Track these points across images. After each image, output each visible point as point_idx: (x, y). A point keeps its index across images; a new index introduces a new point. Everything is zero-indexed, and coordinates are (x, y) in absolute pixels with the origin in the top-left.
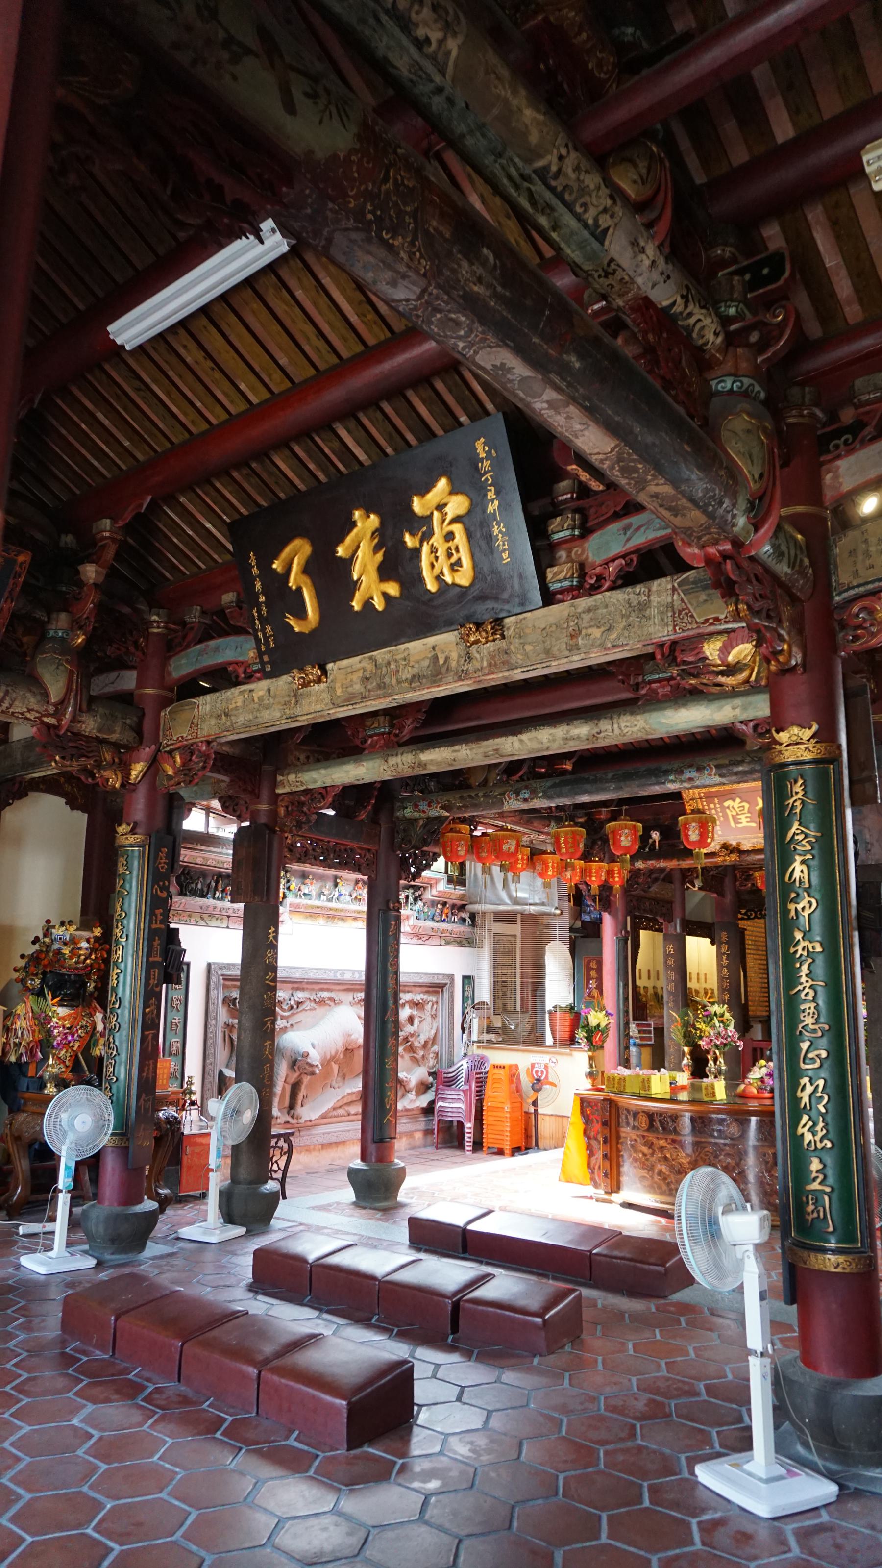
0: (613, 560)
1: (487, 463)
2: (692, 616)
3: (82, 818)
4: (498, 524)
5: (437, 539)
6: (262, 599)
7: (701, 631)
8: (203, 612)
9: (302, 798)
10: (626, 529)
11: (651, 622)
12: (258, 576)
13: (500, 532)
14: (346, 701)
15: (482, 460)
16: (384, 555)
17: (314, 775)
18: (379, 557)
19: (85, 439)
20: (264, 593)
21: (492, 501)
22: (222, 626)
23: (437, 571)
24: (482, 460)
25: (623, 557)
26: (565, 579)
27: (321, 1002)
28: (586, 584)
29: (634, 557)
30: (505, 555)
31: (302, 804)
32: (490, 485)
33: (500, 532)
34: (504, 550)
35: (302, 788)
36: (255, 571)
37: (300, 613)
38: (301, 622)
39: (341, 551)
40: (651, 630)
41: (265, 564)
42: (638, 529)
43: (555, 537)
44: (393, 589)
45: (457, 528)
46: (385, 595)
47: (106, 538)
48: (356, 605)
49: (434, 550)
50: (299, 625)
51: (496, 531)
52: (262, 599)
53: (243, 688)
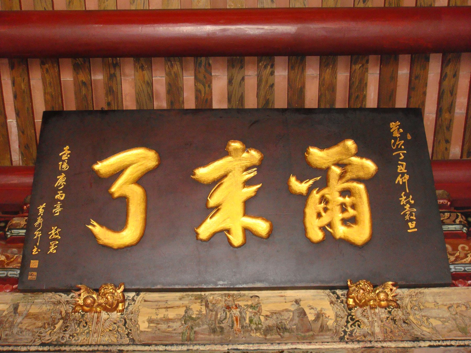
4: (407, 195)
5: (333, 192)
12: (65, 172)
14: (154, 338)
15: (395, 138)
18: (251, 190)
21: (403, 174)
23: (325, 219)
27: (298, 343)
30: (412, 225)
32: (402, 161)
33: (408, 202)
34: (411, 220)
44: (261, 226)
46: (247, 231)
48: (396, 182)
52: (60, 196)
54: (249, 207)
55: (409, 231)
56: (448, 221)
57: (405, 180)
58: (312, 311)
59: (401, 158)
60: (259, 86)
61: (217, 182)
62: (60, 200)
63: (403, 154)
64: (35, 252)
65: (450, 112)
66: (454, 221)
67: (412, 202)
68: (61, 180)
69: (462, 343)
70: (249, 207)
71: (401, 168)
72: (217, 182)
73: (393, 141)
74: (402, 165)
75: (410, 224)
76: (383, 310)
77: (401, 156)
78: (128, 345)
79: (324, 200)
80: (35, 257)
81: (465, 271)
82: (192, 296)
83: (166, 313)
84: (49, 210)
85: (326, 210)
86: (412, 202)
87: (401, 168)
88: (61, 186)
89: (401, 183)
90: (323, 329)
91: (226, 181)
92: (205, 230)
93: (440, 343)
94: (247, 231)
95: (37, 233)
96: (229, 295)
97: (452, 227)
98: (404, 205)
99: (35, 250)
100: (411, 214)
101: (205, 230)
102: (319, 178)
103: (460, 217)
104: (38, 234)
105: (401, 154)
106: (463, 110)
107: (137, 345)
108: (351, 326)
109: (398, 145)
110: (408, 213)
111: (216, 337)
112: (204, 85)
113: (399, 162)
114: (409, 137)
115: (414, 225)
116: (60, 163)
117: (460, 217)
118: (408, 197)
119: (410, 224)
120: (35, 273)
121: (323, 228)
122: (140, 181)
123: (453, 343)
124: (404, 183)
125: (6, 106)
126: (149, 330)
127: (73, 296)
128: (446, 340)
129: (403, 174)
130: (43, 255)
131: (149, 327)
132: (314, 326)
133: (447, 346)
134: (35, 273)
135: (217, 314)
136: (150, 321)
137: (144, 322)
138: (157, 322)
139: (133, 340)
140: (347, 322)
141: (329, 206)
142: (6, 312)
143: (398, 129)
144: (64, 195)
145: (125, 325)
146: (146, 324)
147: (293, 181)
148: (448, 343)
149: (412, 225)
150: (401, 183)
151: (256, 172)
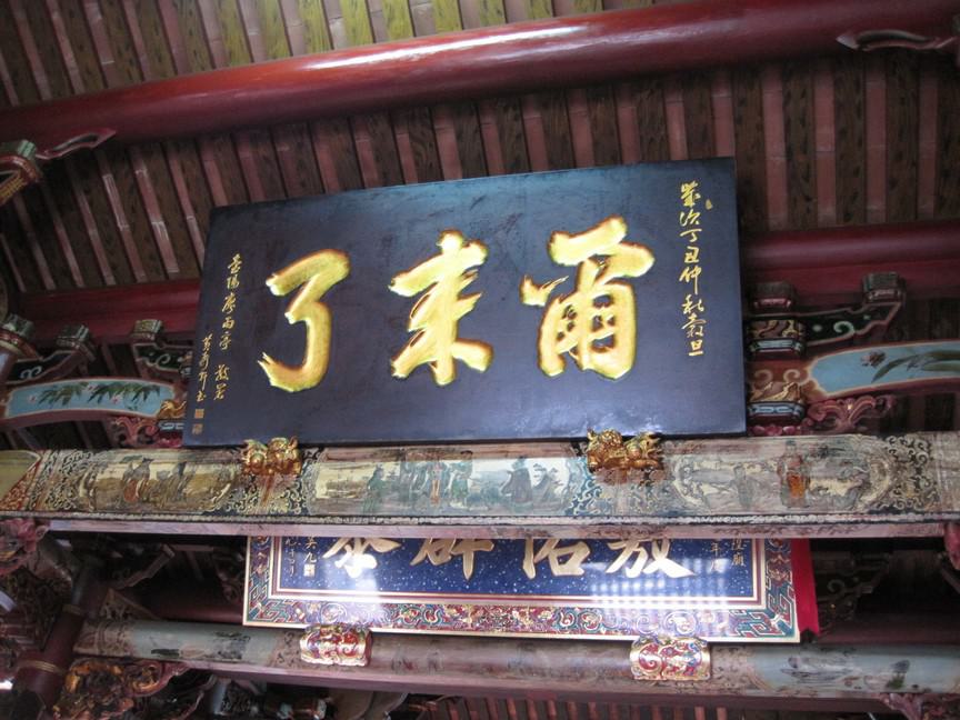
0: (856, 396)
1: (694, 216)
3: (585, 368)
5: (582, 301)
8: (89, 339)
9: (117, 670)
10: (876, 359)
13: (695, 310)
15: (687, 210)
16: (476, 305)
18: (467, 305)
19: (44, 29)
20: (234, 315)
21: (692, 266)
22: (115, 361)
23: (565, 346)
24: (687, 210)
25: (874, 393)
26: (784, 402)
28: (809, 416)
31: (109, 679)
34: (696, 338)
35: (122, 654)
36: (233, 282)
37: (292, 354)
38: (287, 373)
39: (403, 286)
42: (891, 366)
44: (476, 357)
45: (624, 294)
46: (459, 366)
47: (16, 167)
48: (681, 279)
49: (570, 314)
50: (280, 378)
52: (228, 324)
53: (131, 453)
54: (465, 330)
55: (691, 354)
56: (770, 335)
57: (695, 276)
58: (539, 473)
59: (692, 241)
60: (501, 137)
61: (420, 297)
62: (227, 329)
63: (696, 233)
64: (200, 398)
65: (805, 152)
66: (780, 334)
67: (702, 309)
68: (230, 303)
69: (738, 520)
70: (465, 330)
71: (691, 257)
72: (420, 297)
73: (682, 215)
74: (693, 251)
75: (693, 344)
76: (639, 472)
77: (692, 238)
78: (300, 516)
79: (570, 314)
80: (200, 405)
81: (775, 412)
82: (387, 451)
83: (351, 475)
84: (215, 342)
85: (570, 327)
86: (702, 309)
87: (691, 257)
89: (688, 280)
90: (547, 496)
91: (433, 293)
92: (401, 366)
93: (706, 520)
94: (459, 366)
95: (202, 374)
96: (433, 450)
97: (775, 344)
98: (688, 315)
100: (697, 329)
101: (401, 366)
102: (564, 279)
103: (791, 327)
104: (203, 375)
105: (693, 235)
106: (830, 147)
107: (310, 516)
108: (587, 495)
109: (689, 220)
110: (693, 327)
111: (406, 508)
112: (423, 145)
113: (689, 248)
114: (709, 205)
115: (699, 346)
116: (229, 279)
117: (791, 327)
118: (695, 302)
119: (693, 344)
120: (200, 426)
121: (563, 357)
123: (726, 520)
124: (692, 280)
125: (209, 177)
126: (327, 497)
127: (883, 318)
128: (716, 516)
129: (692, 266)
130: (209, 403)
131: (326, 494)
132: (535, 493)
133: (716, 524)
134: (200, 426)
135: (412, 477)
136: (330, 486)
137: (322, 487)
138: (338, 486)
139: (304, 510)
140: (583, 489)
141: (576, 321)
142: (171, 474)
143: (694, 194)
144: (233, 322)
145: (299, 490)
146: (325, 490)
147: (528, 287)
148: (719, 520)
150: (688, 280)
151: (476, 276)
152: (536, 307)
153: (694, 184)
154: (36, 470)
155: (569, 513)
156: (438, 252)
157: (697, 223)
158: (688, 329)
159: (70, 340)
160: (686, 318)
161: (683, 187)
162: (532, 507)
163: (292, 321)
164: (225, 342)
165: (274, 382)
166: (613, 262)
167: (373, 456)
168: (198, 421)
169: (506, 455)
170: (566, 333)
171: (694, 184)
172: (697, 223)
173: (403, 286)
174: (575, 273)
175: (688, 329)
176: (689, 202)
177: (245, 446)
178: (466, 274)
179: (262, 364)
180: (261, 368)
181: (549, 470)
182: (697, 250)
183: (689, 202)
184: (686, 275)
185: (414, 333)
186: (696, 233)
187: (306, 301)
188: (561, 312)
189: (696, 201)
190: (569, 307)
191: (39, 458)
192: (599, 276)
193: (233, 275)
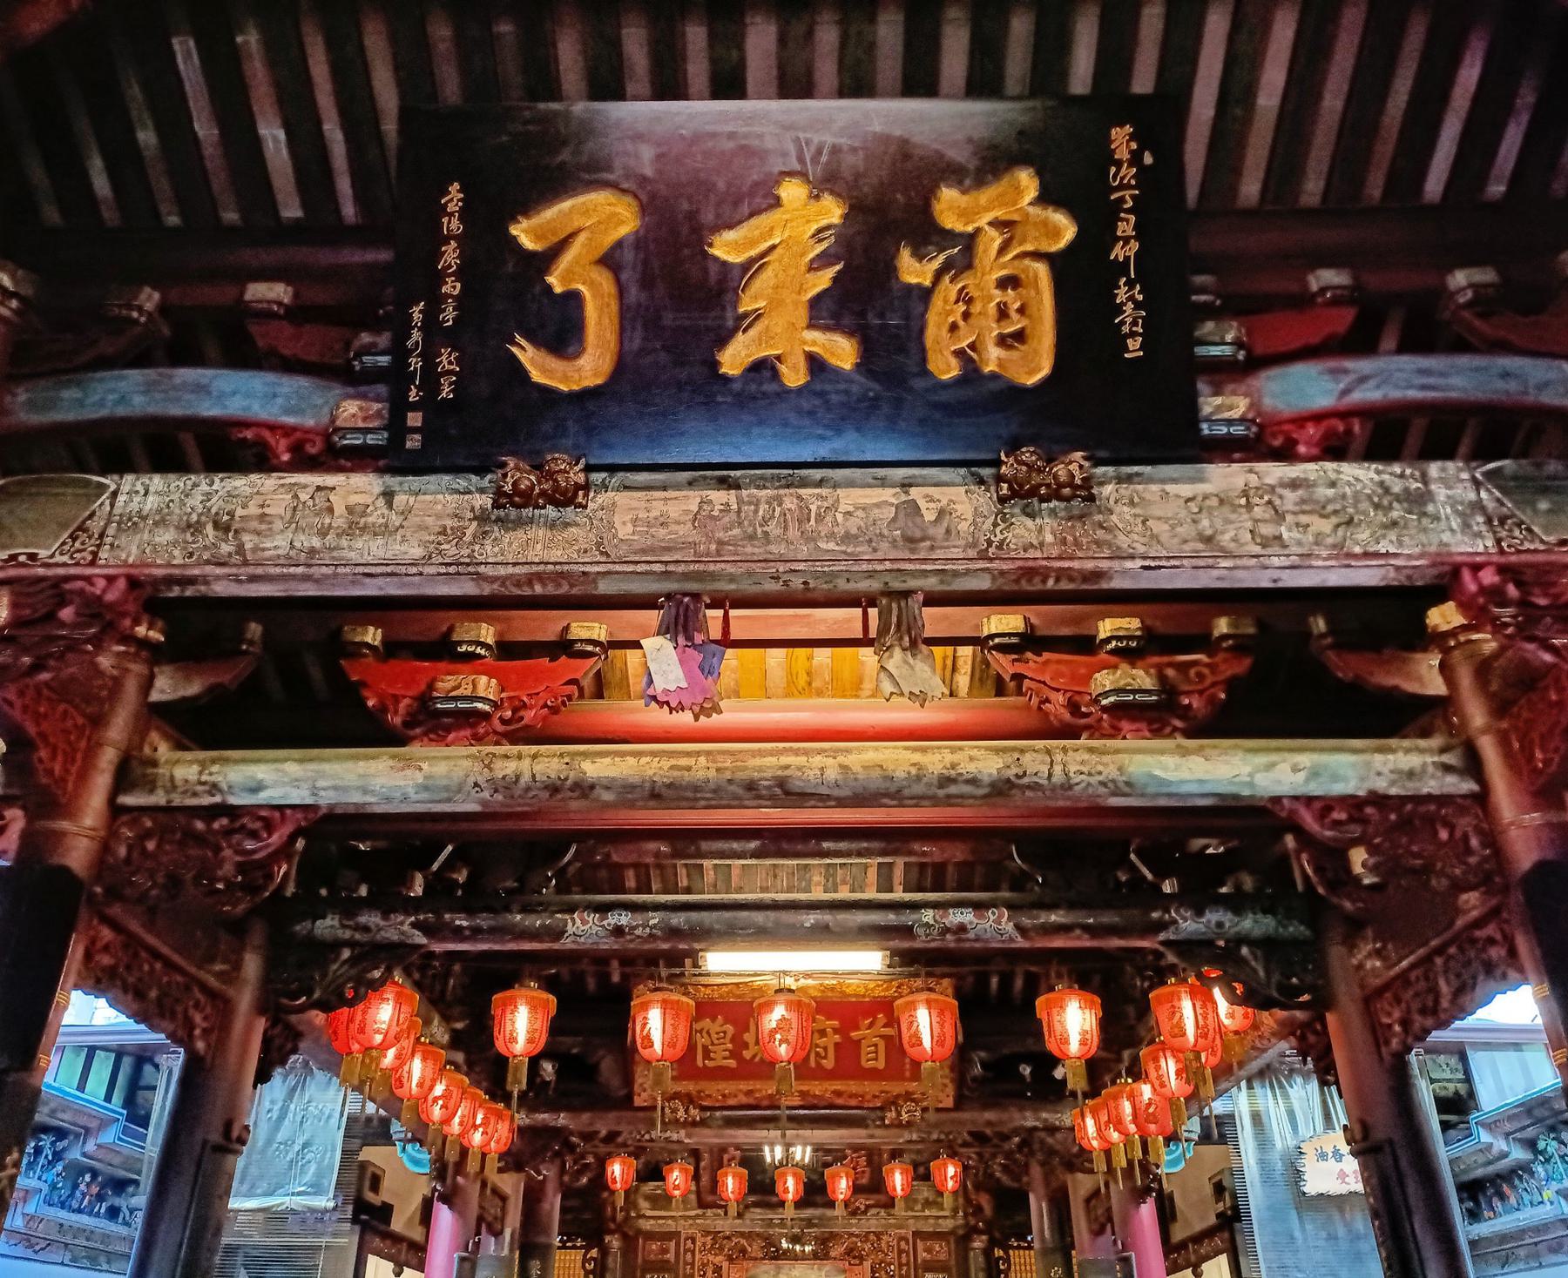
2: (1529, 530)
4: (1130, 284)
6: (452, 287)
7: (1553, 558)
8: (163, 309)
11: (1443, 525)
12: (455, 238)
15: (1119, 164)
17: (261, 772)
18: (823, 280)
20: (460, 275)
21: (1126, 240)
24: (1119, 164)
29: (63, 800)
30: (1134, 344)
32: (1128, 211)
33: (1131, 298)
34: (1133, 334)
36: (454, 225)
37: (562, 332)
38: (553, 363)
39: (727, 247)
40: (1446, 537)
41: (488, 222)
43: (1201, 351)
45: (1042, 270)
46: (816, 364)
49: (965, 298)
51: (1121, 294)
52: (452, 287)
54: (826, 312)
61: (753, 266)
62: (451, 296)
63: (1132, 197)
64: (413, 396)
67: (1140, 298)
70: (826, 312)
71: (1126, 227)
72: (753, 266)
74: (1127, 221)
79: (965, 298)
80: (414, 407)
84: (431, 316)
85: (966, 316)
87: (1126, 227)
88: (450, 266)
94: (816, 364)
95: (413, 360)
99: (413, 392)
100: (1134, 323)
104: (415, 363)
110: (1129, 320)
114: (1148, 159)
118: (1131, 288)
122: (609, 260)
129: (1126, 240)
130: (429, 403)
134: (418, 437)
135: (756, 511)
140: (995, 525)
144: (458, 285)
149: (1134, 344)
152: (919, 286)
153: (1128, 129)
154: (112, 505)
155: (983, 556)
156: (777, 202)
157: (1133, 182)
158: (1123, 323)
159: (130, 307)
160: (1119, 309)
161: (1113, 132)
162: (932, 548)
163: (558, 290)
164: (449, 315)
165: (537, 376)
166: (1019, 231)
167: (691, 484)
168: (415, 430)
169: (883, 483)
170: (961, 323)
171: (1128, 129)
172: (1133, 182)
173: (727, 247)
174: (969, 241)
175: (1123, 323)
176: (1123, 154)
177: (503, 465)
178: (818, 235)
179: (514, 350)
180: (514, 356)
181: (944, 502)
182: (1133, 218)
183: (1123, 154)
184: (1118, 252)
185: (746, 315)
186: (1132, 197)
187: (576, 261)
188: (953, 296)
189: (1132, 152)
190: (963, 288)
191: (113, 487)
192: (1002, 250)
193: (451, 215)
